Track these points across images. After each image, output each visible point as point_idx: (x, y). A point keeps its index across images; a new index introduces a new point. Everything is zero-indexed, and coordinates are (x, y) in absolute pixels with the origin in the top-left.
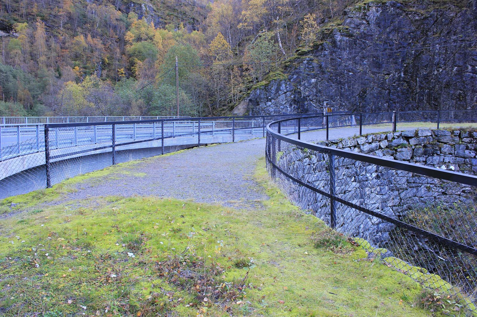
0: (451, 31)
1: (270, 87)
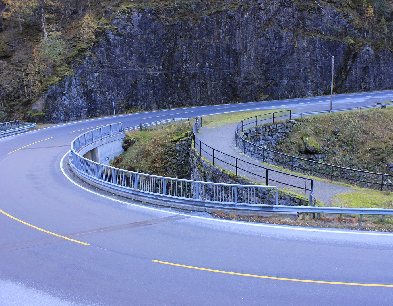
0: (192, 37)
1: (63, 83)
